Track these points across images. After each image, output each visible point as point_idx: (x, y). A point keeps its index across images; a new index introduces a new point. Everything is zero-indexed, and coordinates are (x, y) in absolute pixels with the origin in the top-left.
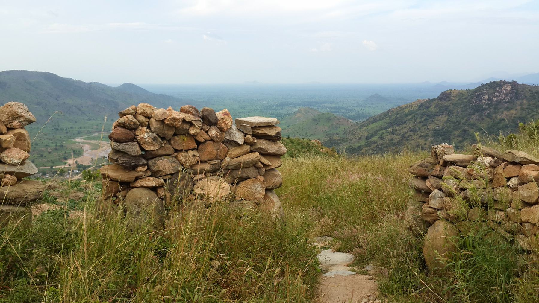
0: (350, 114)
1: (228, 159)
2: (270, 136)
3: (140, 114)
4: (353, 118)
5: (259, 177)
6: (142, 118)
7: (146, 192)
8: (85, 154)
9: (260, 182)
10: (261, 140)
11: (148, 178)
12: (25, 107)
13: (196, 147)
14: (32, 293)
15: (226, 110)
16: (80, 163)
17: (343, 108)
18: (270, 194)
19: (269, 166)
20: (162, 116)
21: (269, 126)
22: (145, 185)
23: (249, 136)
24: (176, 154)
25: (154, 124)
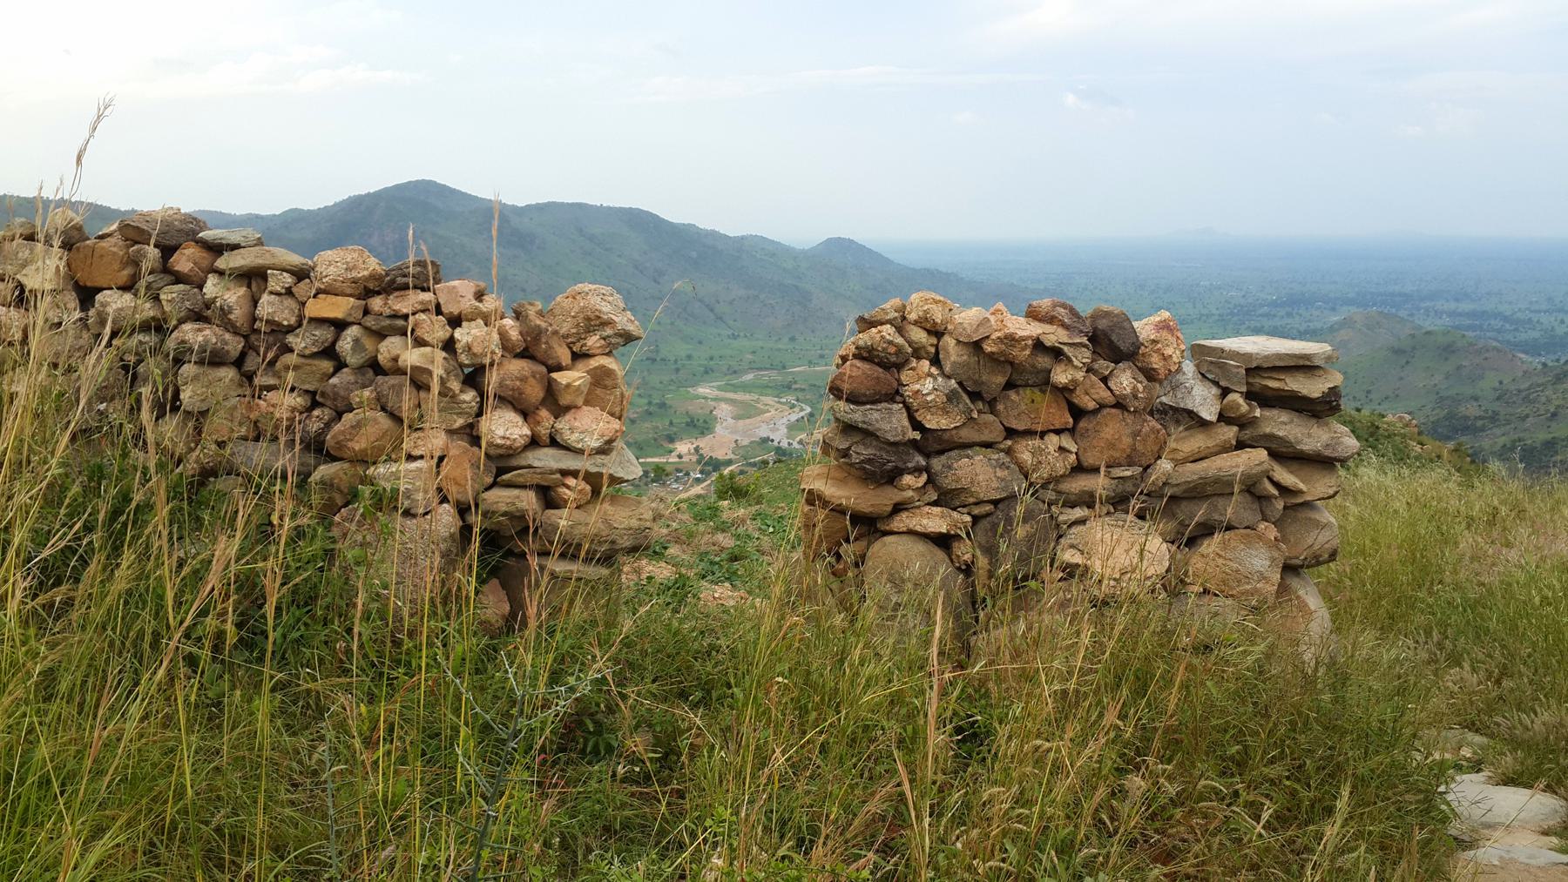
0: (1522, 336)
1: (1165, 465)
2: (1305, 399)
3: (916, 323)
4: (1532, 348)
5: (1262, 526)
6: (919, 336)
7: (921, 547)
8: (718, 428)
9: (1267, 543)
10: (1275, 412)
11: (927, 509)
12: (618, 299)
13: (1070, 426)
14: (623, 805)
15: (1166, 314)
16: (706, 453)
17: (1497, 315)
18: (1294, 582)
19: (1300, 492)
20: (977, 329)
21: (1304, 366)
22: (918, 528)
23: (1235, 397)
24: (1009, 443)
25: (952, 352)
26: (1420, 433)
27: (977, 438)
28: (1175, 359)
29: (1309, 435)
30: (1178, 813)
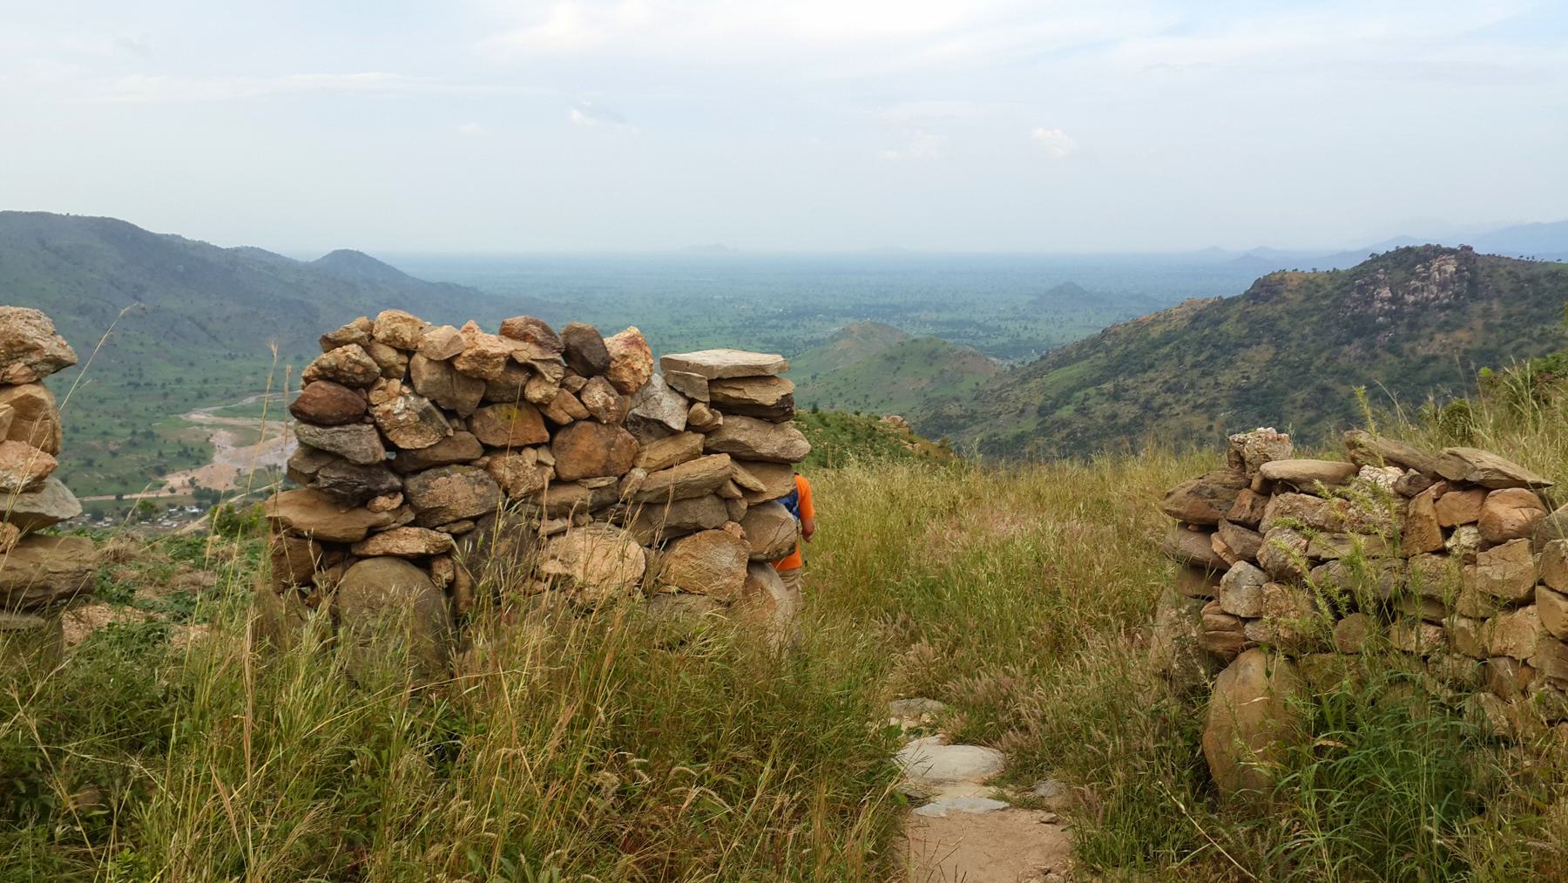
0: (993, 342)
1: (639, 473)
3: (384, 342)
4: (1002, 352)
5: (729, 525)
6: (388, 355)
7: (398, 569)
8: (217, 458)
10: (737, 419)
11: (404, 530)
13: (547, 439)
15: (635, 330)
17: (971, 323)
18: (762, 577)
21: (760, 376)
22: (395, 550)
24: (487, 459)
26: (911, 433)
27: (454, 455)
28: (644, 373)
29: (767, 440)
30: (651, 802)
